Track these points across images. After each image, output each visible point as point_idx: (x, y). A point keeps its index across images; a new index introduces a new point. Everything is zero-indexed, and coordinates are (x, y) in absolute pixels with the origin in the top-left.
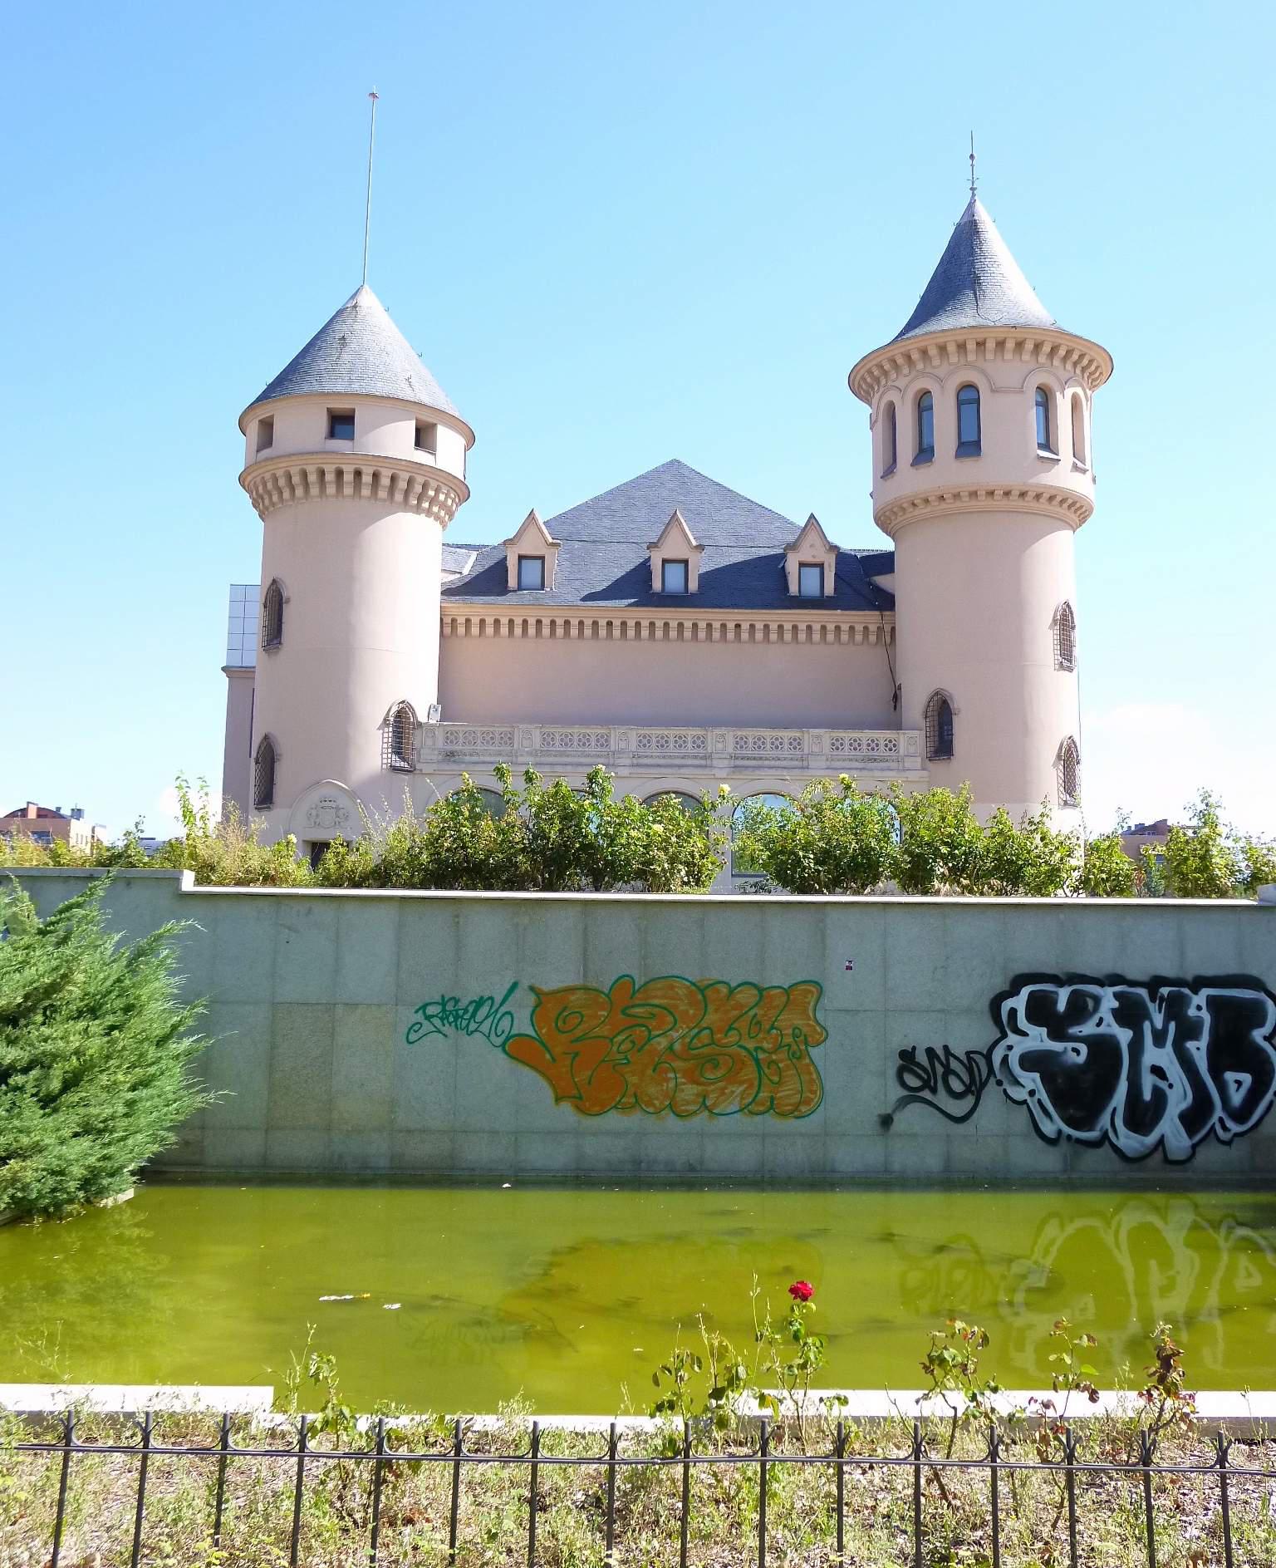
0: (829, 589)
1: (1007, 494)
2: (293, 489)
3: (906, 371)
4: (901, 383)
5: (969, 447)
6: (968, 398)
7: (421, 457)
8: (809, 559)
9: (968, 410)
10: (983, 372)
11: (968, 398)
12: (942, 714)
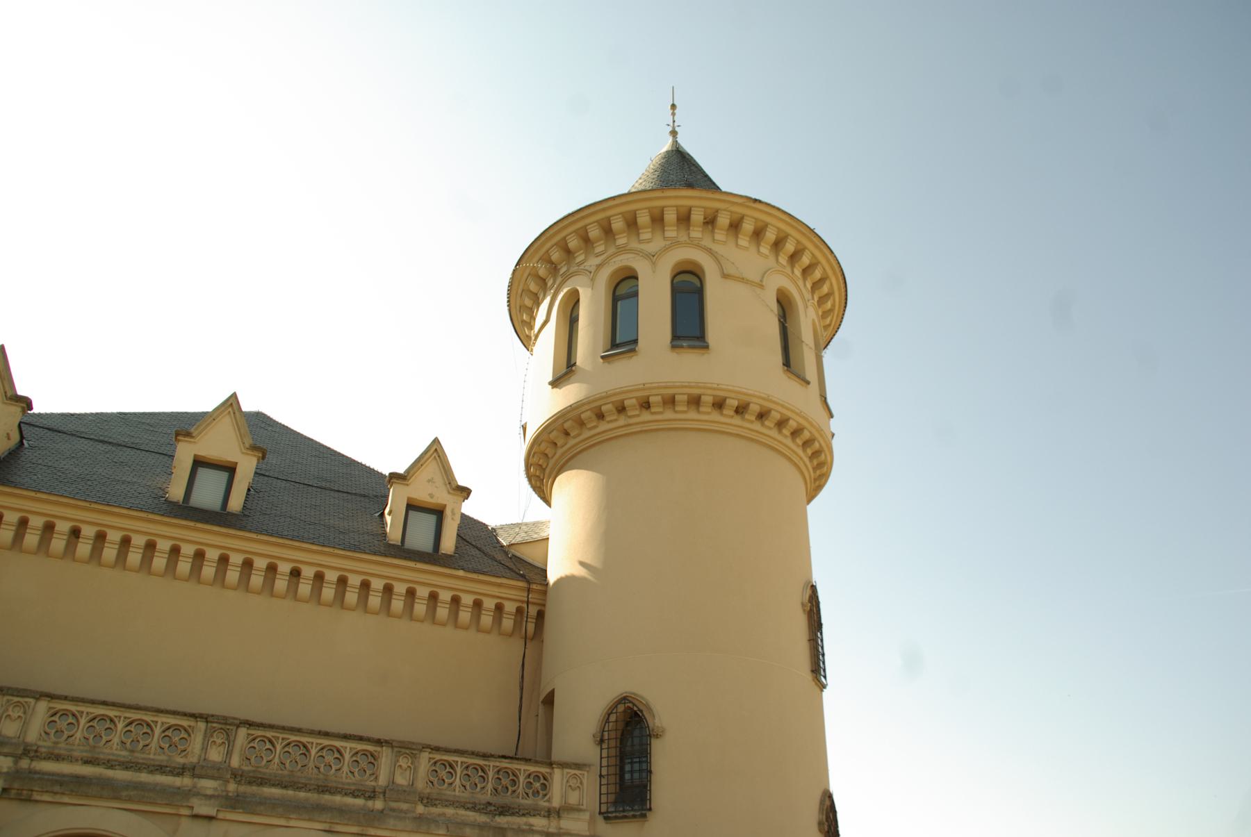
0: (236, 503)
1: (719, 405)
3: (600, 248)
10: (710, 251)
12: (630, 731)
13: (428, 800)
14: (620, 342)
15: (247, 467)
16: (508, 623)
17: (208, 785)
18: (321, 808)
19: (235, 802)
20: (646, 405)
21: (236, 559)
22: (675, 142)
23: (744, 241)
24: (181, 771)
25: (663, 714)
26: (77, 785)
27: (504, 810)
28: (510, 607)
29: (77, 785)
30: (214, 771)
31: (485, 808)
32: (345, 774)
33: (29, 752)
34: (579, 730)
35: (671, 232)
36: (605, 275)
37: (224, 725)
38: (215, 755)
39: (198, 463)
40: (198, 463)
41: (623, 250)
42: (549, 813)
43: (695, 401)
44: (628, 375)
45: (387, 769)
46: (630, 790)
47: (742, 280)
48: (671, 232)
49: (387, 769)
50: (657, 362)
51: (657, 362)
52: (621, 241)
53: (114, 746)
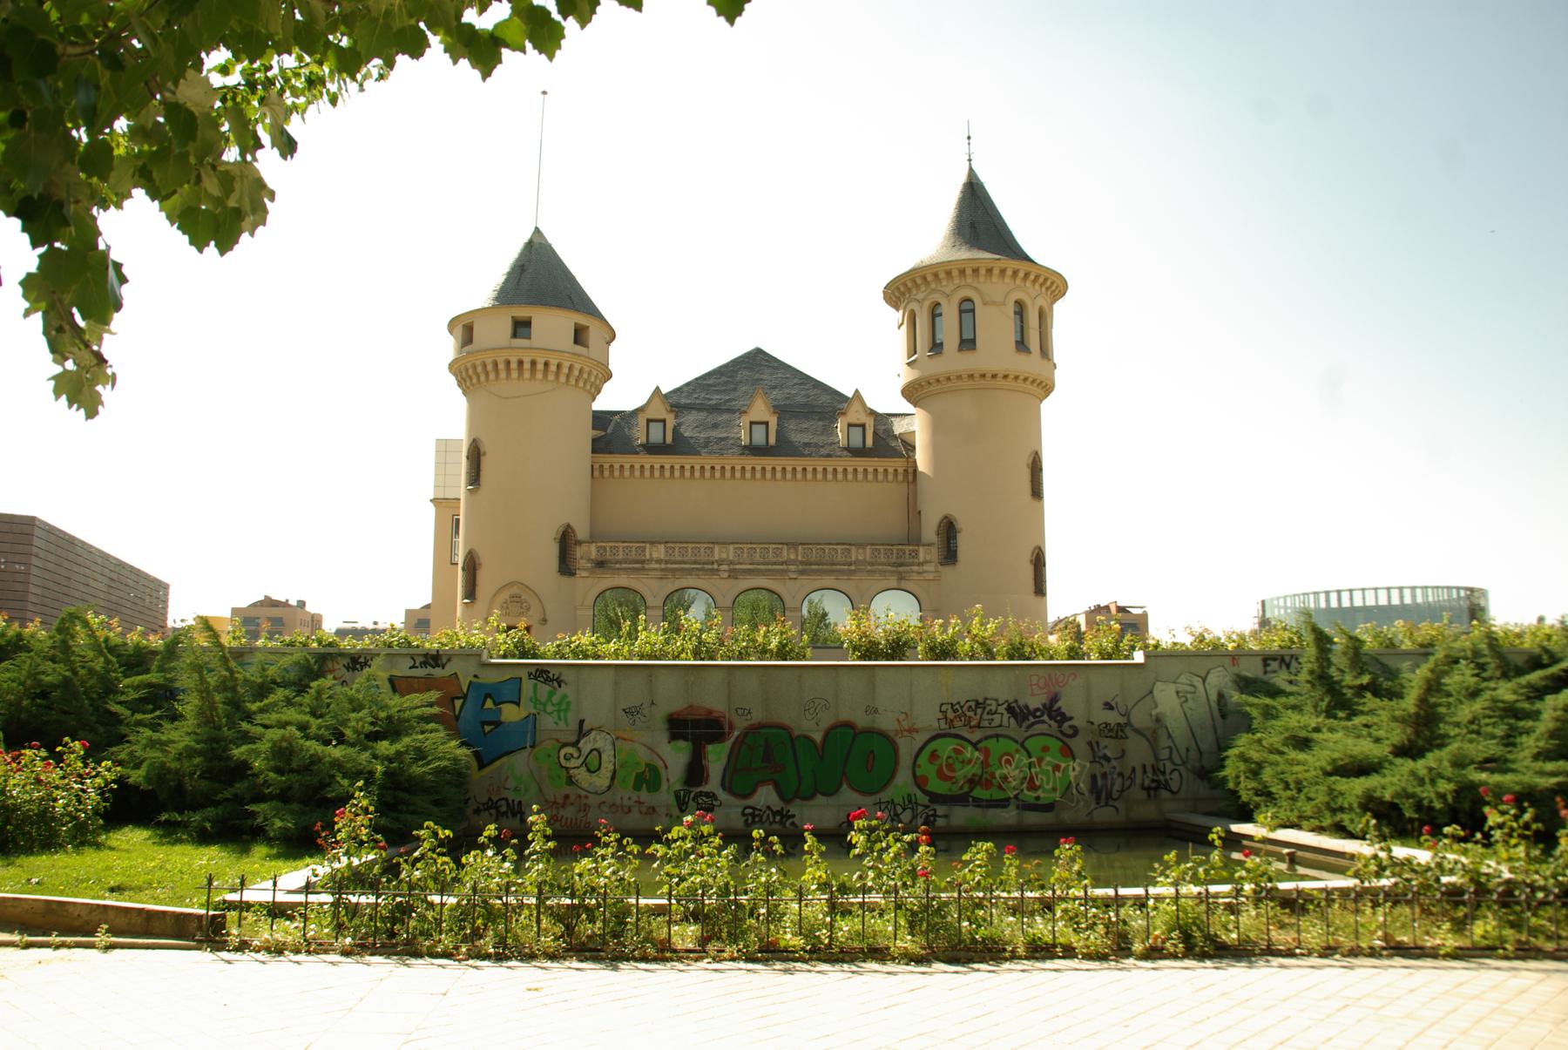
0: (869, 442)
2: (487, 374)
4: (920, 296)
5: (968, 344)
6: (967, 309)
7: (578, 349)
8: (855, 421)
9: (967, 317)
11: (967, 309)
12: (949, 530)
13: (872, 564)
14: (936, 347)
15: (773, 421)
16: (900, 478)
17: (792, 568)
18: (832, 571)
19: (802, 572)
20: (949, 379)
21: (830, 469)
22: (971, 170)
23: (995, 279)
24: (782, 563)
25: (961, 523)
26: (750, 572)
27: (901, 565)
28: (901, 470)
29: (750, 572)
30: (794, 562)
31: (893, 565)
32: (840, 558)
33: (732, 563)
34: (930, 531)
35: (957, 281)
36: (927, 304)
37: (793, 545)
38: (792, 557)
39: (649, 421)
40: (649, 421)
41: (934, 291)
42: (920, 564)
43: (994, 376)
44: (940, 366)
45: (855, 554)
46: (950, 555)
47: (994, 303)
48: (957, 281)
49: (855, 554)
50: (953, 361)
51: (953, 361)
52: (933, 286)
53: (757, 557)
